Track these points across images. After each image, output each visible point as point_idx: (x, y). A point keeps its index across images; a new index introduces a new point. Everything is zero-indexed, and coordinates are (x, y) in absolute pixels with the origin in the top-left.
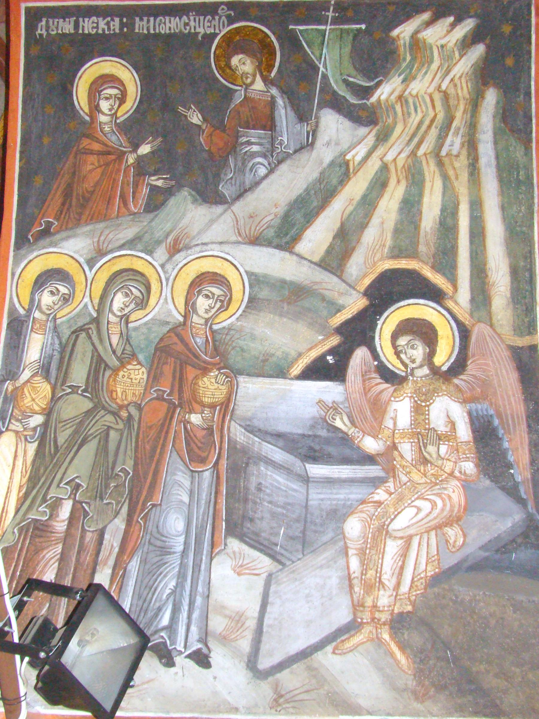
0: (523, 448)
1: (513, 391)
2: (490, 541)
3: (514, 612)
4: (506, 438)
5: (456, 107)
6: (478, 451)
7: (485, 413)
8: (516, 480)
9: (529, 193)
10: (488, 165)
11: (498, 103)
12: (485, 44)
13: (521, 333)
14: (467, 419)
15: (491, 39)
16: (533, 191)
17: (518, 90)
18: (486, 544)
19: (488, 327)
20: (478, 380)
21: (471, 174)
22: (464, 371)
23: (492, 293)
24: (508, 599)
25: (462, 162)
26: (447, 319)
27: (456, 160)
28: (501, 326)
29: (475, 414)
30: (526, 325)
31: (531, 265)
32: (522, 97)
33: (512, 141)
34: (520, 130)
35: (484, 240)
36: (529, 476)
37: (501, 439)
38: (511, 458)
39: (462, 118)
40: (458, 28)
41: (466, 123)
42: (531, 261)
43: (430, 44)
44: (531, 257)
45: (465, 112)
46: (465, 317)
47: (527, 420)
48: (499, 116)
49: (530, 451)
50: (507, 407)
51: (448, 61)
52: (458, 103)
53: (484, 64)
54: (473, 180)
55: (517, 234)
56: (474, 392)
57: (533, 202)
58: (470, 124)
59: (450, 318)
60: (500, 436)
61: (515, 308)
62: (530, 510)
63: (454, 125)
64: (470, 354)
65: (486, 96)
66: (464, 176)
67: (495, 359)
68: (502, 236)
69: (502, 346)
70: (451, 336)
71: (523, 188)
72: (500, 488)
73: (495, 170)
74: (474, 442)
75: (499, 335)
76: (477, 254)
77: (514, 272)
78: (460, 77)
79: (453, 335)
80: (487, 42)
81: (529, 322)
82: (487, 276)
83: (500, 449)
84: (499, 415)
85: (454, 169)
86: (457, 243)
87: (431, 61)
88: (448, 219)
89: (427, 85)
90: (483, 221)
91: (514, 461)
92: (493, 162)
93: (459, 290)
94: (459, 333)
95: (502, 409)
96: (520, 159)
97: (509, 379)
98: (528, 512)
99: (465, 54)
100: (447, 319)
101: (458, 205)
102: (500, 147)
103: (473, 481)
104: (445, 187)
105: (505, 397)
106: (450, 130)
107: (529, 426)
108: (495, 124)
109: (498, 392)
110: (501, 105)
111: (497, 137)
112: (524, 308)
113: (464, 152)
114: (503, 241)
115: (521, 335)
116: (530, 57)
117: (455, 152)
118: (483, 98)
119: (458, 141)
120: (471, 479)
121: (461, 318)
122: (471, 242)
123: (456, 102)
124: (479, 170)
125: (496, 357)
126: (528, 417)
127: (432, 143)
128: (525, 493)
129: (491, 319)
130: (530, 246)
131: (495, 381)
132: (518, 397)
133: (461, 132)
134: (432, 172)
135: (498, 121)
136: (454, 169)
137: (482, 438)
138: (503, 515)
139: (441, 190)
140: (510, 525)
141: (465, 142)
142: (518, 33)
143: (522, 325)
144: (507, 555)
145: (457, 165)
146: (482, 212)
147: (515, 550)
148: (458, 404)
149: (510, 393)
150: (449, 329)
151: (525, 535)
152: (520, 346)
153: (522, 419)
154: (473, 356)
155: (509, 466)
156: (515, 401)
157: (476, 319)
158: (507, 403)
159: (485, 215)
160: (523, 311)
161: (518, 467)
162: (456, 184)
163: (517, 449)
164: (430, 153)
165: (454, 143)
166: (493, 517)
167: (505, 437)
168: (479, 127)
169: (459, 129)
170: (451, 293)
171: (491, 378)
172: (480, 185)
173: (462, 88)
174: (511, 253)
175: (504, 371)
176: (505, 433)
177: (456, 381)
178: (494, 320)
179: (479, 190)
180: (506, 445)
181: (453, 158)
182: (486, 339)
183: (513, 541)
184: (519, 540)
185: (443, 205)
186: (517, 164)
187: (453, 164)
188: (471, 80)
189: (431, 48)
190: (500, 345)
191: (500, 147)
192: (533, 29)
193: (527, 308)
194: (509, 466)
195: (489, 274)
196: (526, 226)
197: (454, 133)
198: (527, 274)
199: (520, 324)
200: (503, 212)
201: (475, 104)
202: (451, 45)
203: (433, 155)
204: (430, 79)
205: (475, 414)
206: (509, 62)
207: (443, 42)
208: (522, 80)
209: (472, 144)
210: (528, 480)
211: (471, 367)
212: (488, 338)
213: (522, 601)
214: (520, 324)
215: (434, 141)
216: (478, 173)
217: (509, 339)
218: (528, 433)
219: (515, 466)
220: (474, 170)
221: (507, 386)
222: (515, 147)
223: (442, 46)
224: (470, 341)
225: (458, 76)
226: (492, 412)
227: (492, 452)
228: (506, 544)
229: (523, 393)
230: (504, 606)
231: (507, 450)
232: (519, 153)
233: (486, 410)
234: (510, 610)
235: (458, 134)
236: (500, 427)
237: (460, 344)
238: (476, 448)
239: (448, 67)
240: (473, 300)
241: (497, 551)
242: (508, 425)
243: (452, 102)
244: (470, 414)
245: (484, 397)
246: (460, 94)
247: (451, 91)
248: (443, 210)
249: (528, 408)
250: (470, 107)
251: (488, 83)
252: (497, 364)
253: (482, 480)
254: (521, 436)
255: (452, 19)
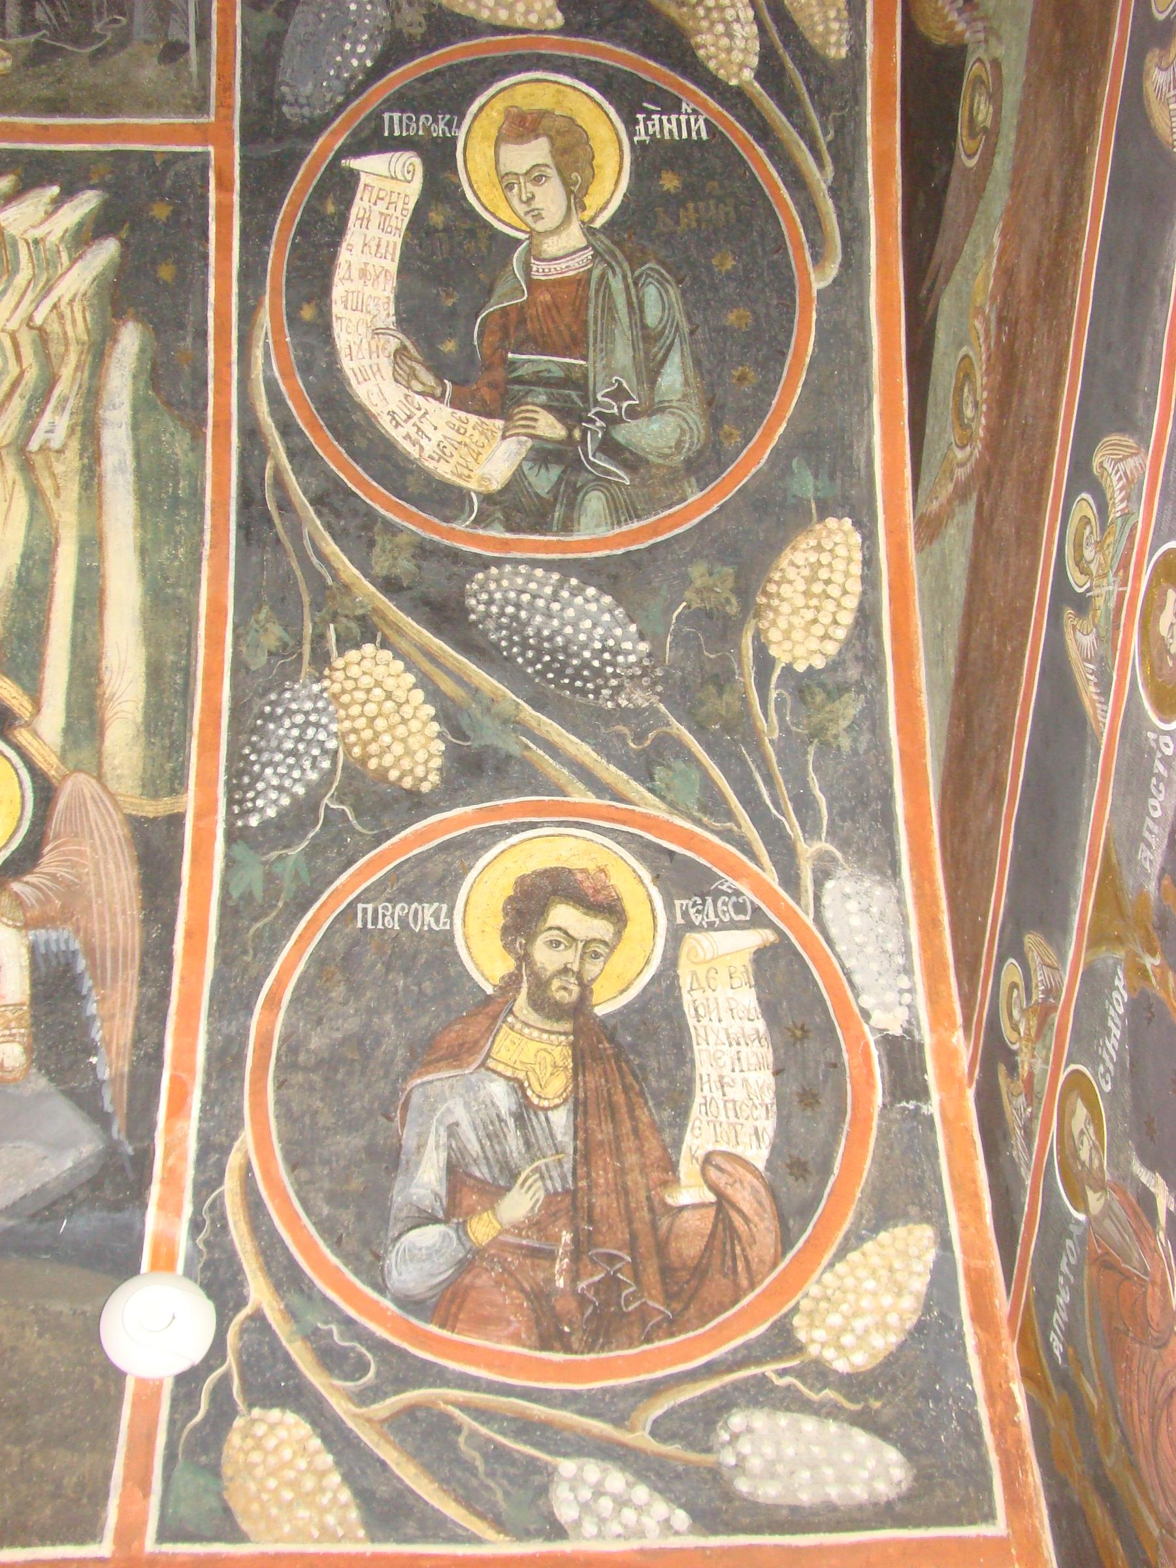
0: (125, 1015)
1: (123, 904)
2: (24, 1197)
3: (40, 1335)
4: (94, 996)
5: (63, 357)
6: (36, 1021)
7: (63, 947)
8: (100, 1076)
9: (195, 521)
10: (120, 469)
11: (142, 350)
12: (120, 240)
13: (156, 791)
14: (25, 960)
15: (132, 230)
16: (203, 518)
17: (181, 326)
18: (14, 1204)
19: (93, 781)
20: (59, 883)
21: (86, 486)
22: (35, 866)
23: (108, 714)
24: (34, 1312)
25: (69, 465)
26: (13, 766)
27: (58, 460)
28: (119, 777)
29: (42, 950)
30: (167, 776)
31: (189, 661)
32: (189, 340)
33: (169, 423)
34: (184, 403)
35: (101, 614)
36: (126, 1069)
37: (84, 997)
38: (97, 1034)
39: (74, 379)
40: (66, 207)
41: (80, 387)
42: (189, 653)
43: (13, 237)
44: (189, 645)
45: (79, 367)
46: (48, 762)
47: (142, 960)
48: (145, 377)
49: (137, 1019)
50: (108, 936)
51: (47, 269)
52: (67, 350)
53: (117, 277)
54: (88, 498)
55: (166, 602)
56: (48, 908)
57: (202, 541)
58: (89, 390)
59: (19, 764)
60: (85, 991)
61: (150, 744)
62: (115, 1135)
63: (57, 392)
64: (51, 834)
65: (120, 337)
66: (72, 490)
67: (98, 842)
68: (138, 605)
69: (115, 817)
70: (18, 800)
71: (184, 513)
72: (64, 1092)
73: (131, 478)
74: (31, 1005)
75: (112, 796)
76: (85, 640)
77: (155, 673)
78: (72, 301)
79: (23, 797)
80: (124, 234)
81: (174, 770)
82: (101, 682)
83: (78, 1018)
84: (90, 952)
85: (53, 476)
86: (48, 619)
87: (14, 271)
88: (35, 572)
89: (7, 315)
90: (103, 576)
91: (103, 1039)
92: (130, 463)
93: (43, 710)
94: (35, 792)
95: (96, 941)
96: (181, 457)
97: (119, 880)
98: (110, 1137)
99: (80, 257)
100: (13, 766)
101: (57, 545)
102: (143, 435)
103: (15, 1080)
104: (33, 510)
105: (107, 917)
106: (48, 402)
107: (143, 972)
108: (136, 391)
109: (95, 906)
110: (149, 355)
111: (140, 416)
112: (167, 742)
113: (75, 445)
114: (137, 613)
115: (156, 796)
116: (207, 265)
117: (56, 444)
118: (115, 341)
119: (63, 423)
120: (10, 1077)
121: (41, 764)
122: (77, 617)
123: (62, 349)
124: (100, 477)
125: (101, 837)
126: (144, 954)
127: (13, 428)
128: (112, 1101)
129: (100, 765)
130: (190, 624)
131: (92, 887)
132: (132, 916)
133: (69, 406)
134: (10, 483)
135: (142, 384)
136: (53, 476)
137: (47, 998)
138: (59, 1146)
139: (26, 516)
140: (69, 1164)
141: (76, 424)
142: (184, 219)
143: (160, 776)
144: (52, 1223)
145: (59, 468)
146: (102, 560)
147: (70, 1213)
148: (13, 931)
149: (118, 908)
150: (17, 785)
151: (95, 1184)
152: (151, 816)
153: (133, 960)
154: (57, 837)
155: (91, 1049)
156: (125, 923)
157: (71, 765)
158: (108, 929)
159: (106, 565)
160: (163, 748)
161: (109, 1051)
162: (55, 505)
163: (112, 1017)
164: (8, 445)
165: (56, 426)
166: (40, 1151)
167: (93, 993)
168: (105, 399)
169: (66, 400)
170: (26, 716)
171: (85, 879)
172: (101, 507)
173: (74, 321)
174: (152, 639)
175: (111, 866)
176: (95, 985)
177: (16, 886)
178: (106, 768)
179: (100, 517)
180: (92, 1008)
181: (53, 456)
182: (85, 804)
183: (71, 1195)
184: (81, 1195)
185: (26, 546)
186: (176, 470)
187: (50, 467)
188: (91, 305)
189: (15, 245)
190: (110, 815)
191: (143, 435)
192: (212, 213)
193: (172, 743)
194: (91, 1049)
195: (106, 679)
196: (185, 587)
197: (56, 407)
198: (179, 679)
199: (156, 773)
200: (143, 559)
201: (99, 352)
202: (54, 239)
203: (13, 450)
204: (13, 305)
205: (42, 950)
206: (166, 272)
207: (38, 233)
208: (191, 309)
209: (89, 430)
210: (122, 1076)
211: (50, 862)
212: (89, 801)
213: (61, 1313)
214: (156, 773)
215: (16, 423)
216: (100, 484)
217: (132, 804)
218: (141, 986)
219: (103, 1050)
220: (92, 478)
221: (113, 895)
222: (172, 434)
223: (36, 242)
224: (53, 809)
225: (66, 299)
226: (76, 945)
227: (61, 1023)
228: (54, 1203)
229: (143, 908)
230: (22, 1325)
231: (93, 1018)
232: (179, 446)
233: (67, 942)
234: (31, 1334)
235: (64, 409)
236: (87, 975)
237: (34, 815)
238: (33, 1016)
239: (48, 280)
240: (68, 730)
241: (33, 1217)
242: (104, 970)
243: (55, 348)
244: (33, 949)
245: (65, 916)
246: (70, 334)
247: (54, 328)
248: (27, 556)
249: (148, 934)
250: (90, 358)
251: (125, 313)
252: (100, 852)
253: (33, 1078)
254: (124, 989)
255: (55, 190)
